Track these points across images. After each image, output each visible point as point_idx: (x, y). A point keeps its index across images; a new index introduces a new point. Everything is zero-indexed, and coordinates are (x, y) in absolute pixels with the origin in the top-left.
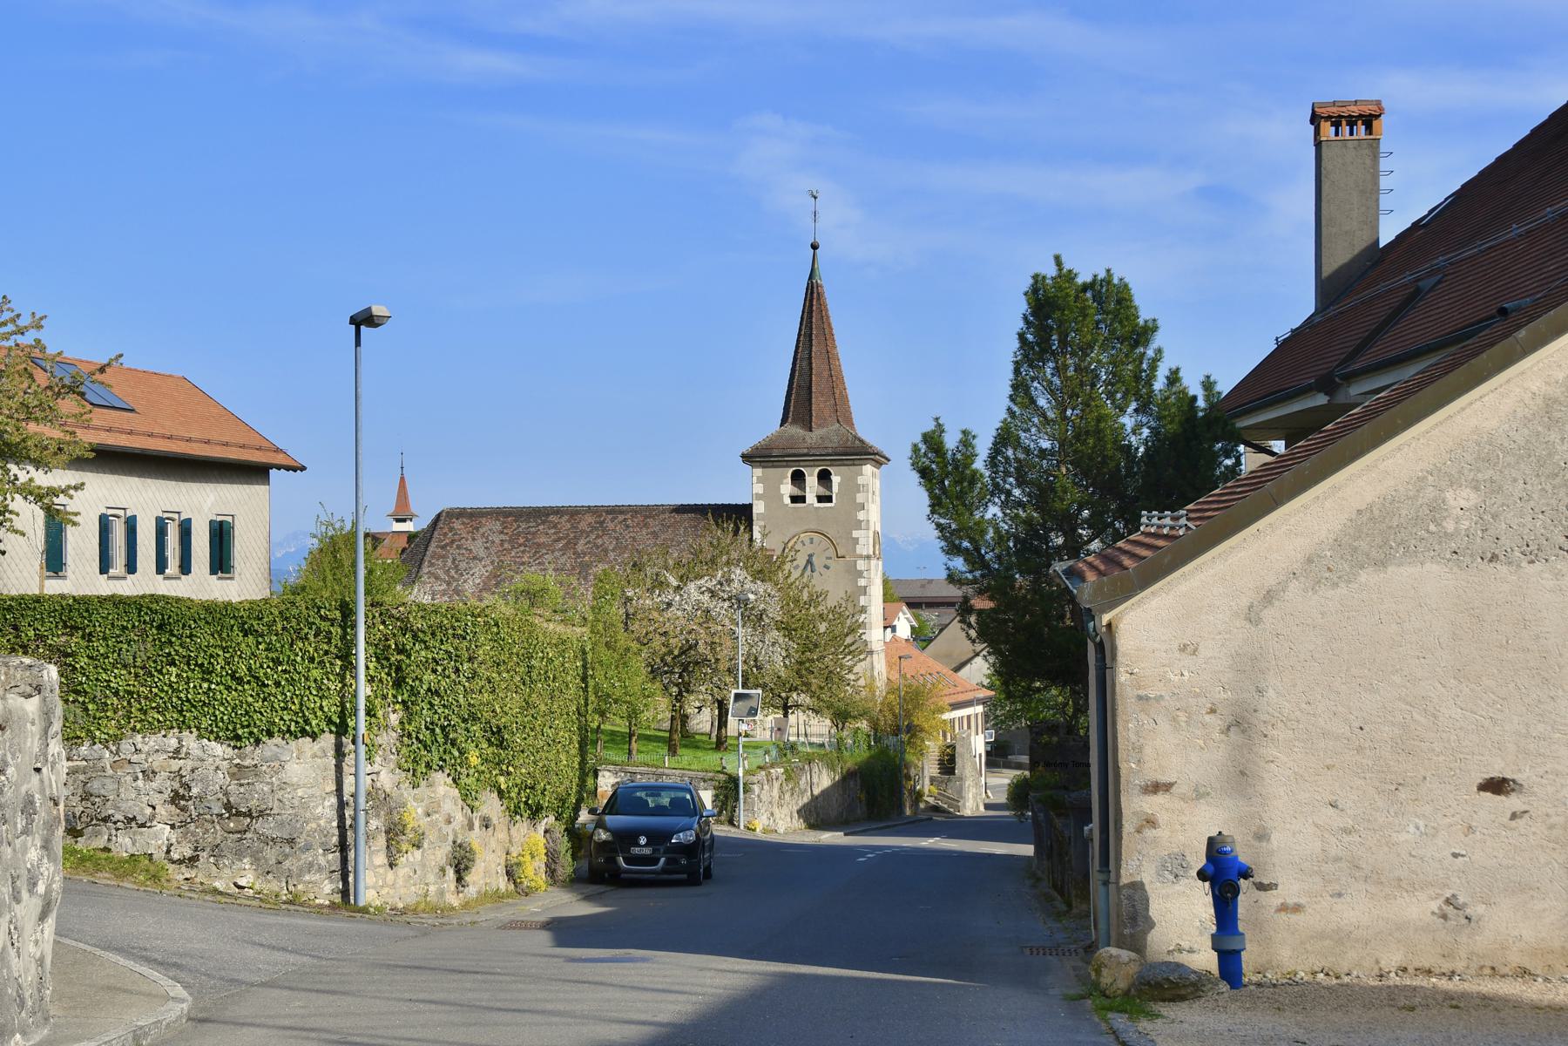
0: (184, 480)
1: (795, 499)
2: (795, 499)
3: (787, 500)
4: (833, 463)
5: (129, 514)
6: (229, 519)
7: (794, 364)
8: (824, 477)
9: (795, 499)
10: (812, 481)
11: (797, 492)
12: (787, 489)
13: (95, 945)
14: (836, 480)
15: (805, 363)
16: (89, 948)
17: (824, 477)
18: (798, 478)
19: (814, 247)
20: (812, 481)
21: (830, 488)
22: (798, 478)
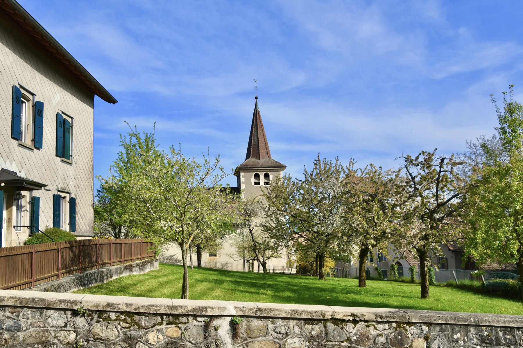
0: (38, 70)
1: (256, 184)
2: (256, 184)
3: (253, 184)
4: (270, 170)
5: (37, 99)
6: (69, 120)
7: (237, 272)
8: (266, 176)
9: (256, 184)
10: (262, 177)
11: (256, 181)
12: (253, 180)
13: (394, 272)
14: (271, 177)
15: (256, 137)
16: (396, 272)
17: (266, 176)
18: (257, 176)
19: (256, 98)
20: (262, 177)
21: (269, 180)
22: (257, 176)
